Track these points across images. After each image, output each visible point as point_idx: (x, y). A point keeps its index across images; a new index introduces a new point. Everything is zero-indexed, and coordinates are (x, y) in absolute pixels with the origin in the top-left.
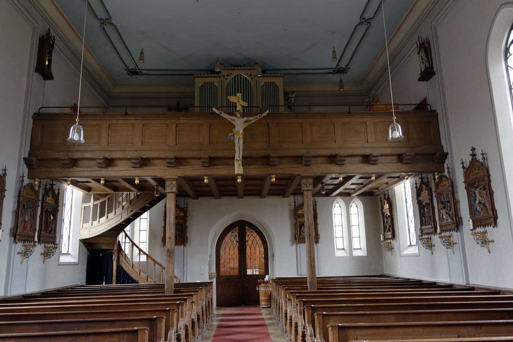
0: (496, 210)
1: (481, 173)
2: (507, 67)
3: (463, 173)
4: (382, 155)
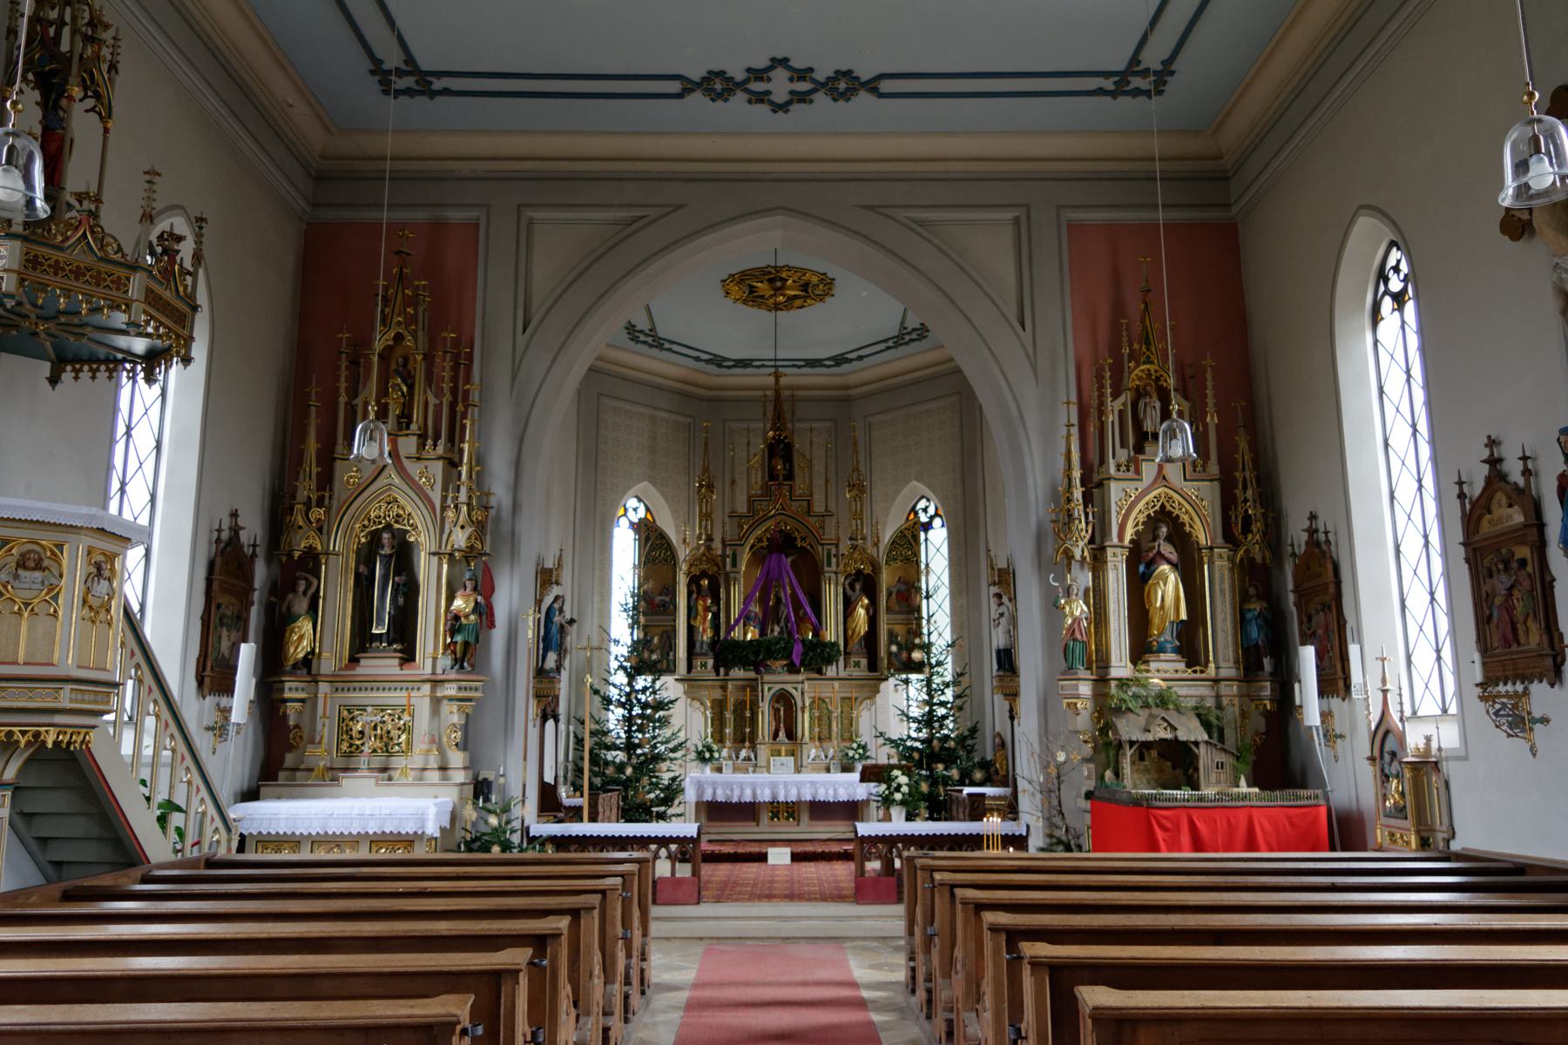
0: (1561, 635)
1: (1517, 517)
2: (1376, 342)
3: (1459, 514)
4: (1403, 322)
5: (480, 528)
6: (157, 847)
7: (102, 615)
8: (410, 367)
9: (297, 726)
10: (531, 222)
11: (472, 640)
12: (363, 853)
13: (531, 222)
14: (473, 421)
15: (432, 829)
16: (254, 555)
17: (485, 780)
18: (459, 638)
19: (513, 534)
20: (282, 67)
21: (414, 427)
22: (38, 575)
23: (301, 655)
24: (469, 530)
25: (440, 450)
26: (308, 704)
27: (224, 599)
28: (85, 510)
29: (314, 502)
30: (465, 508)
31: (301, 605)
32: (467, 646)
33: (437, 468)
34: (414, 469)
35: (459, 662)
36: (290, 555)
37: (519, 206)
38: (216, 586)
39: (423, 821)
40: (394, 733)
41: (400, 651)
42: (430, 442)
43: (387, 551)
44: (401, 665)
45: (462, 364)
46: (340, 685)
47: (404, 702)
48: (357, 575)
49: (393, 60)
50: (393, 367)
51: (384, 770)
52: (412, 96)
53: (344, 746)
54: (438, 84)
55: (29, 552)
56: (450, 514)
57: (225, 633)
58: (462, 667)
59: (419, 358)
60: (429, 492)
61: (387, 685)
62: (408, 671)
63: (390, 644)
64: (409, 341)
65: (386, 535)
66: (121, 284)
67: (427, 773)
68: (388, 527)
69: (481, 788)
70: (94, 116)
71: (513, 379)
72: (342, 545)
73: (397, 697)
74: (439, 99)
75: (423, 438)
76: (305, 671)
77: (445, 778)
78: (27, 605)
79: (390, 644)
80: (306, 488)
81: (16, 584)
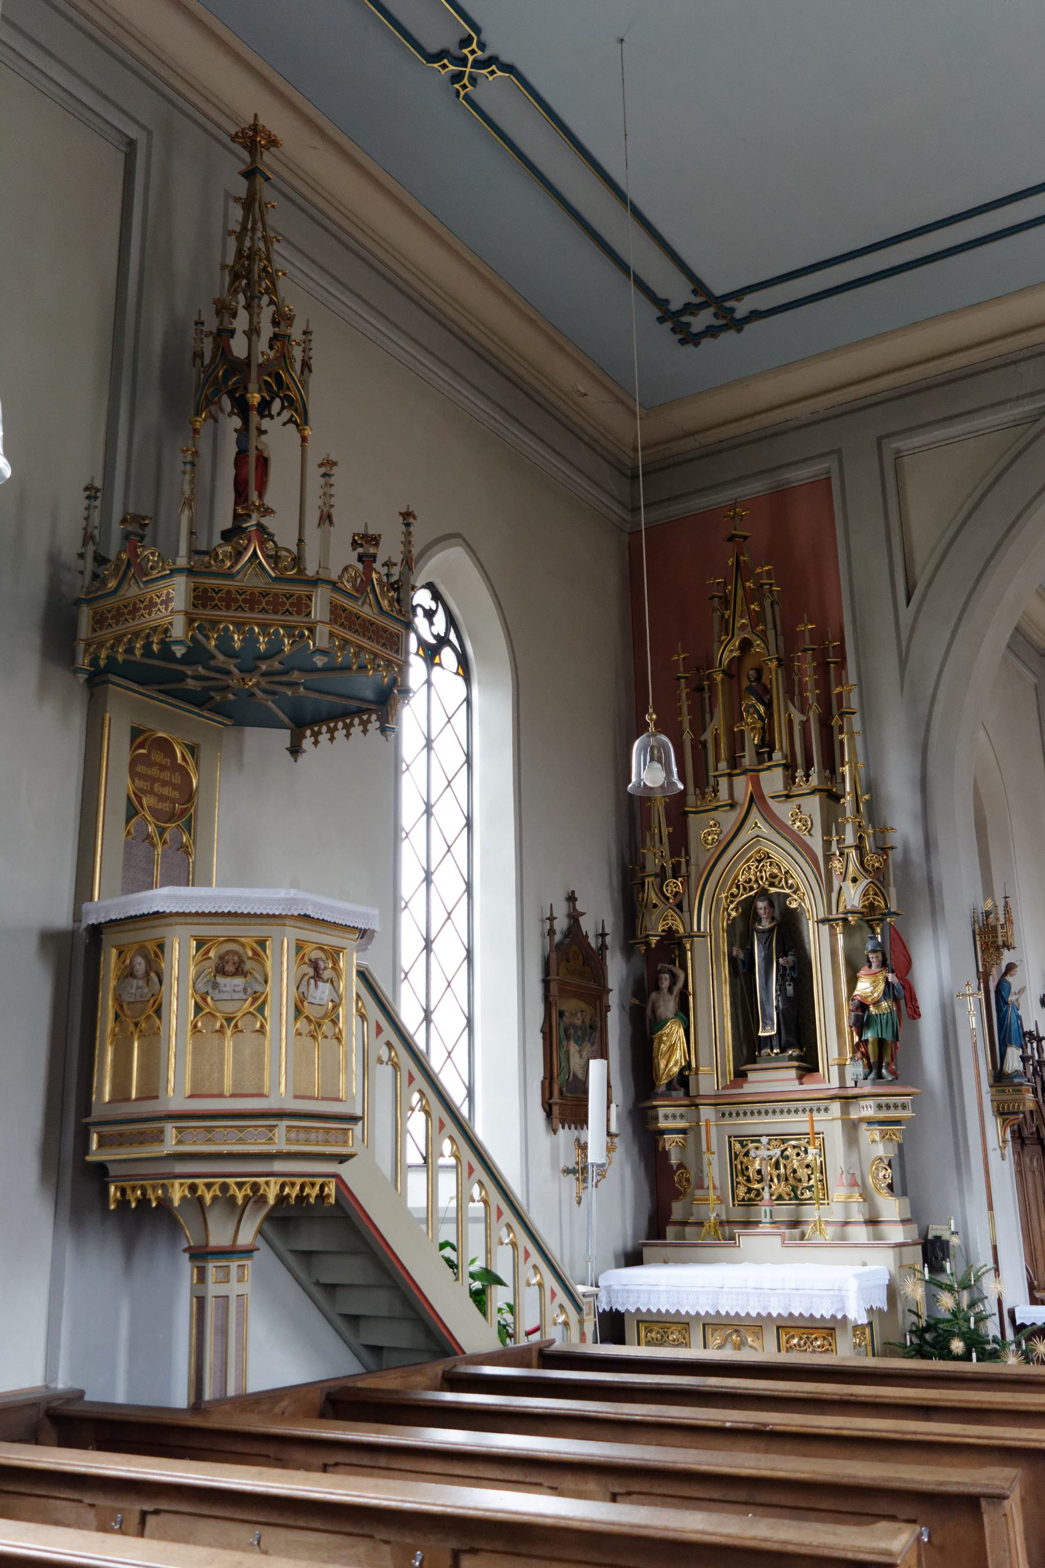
5: (879, 878)
6: (473, 1333)
7: (327, 1027)
8: (765, 680)
9: (681, 1166)
10: (898, 456)
11: (888, 1036)
12: (764, 1351)
13: (898, 456)
14: (851, 738)
15: (857, 1314)
16: (603, 947)
17: (938, 1238)
18: (869, 1035)
19: (930, 882)
20: (561, 349)
21: (777, 756)
22: (239, 981)
23: (676, 1069)
24: (863, 883)
25: (814, 781)
26: (691, 1136)
27: (570, 1005)
28: (282, 893)
29: (669, 872)
30: (853, 853)
31: (668, 1005)
32: (885, 1047)
33: (813, 805)
34: (784, 811)
35: (875, 1068)
36: (648, 944)
37: (880, 440)
38: (554, 988)
39: (842, 1300)
40: (802, 1173)
41: (799, 1058)
42: (800, 773)
43: (765, 924)
44: (800, 1078)
45: (830, 662)
46: (727, 1109)
47: (806, 1128)
48: (732, 961)
49: (679, 293)
50: (745, 683)
51: (795, 1224)
52: (714, 336)
53: (741, 1191)
54: (742, 308)
55: (228, 952)
56: (836, 864)
57: (573, 1048)
58: (880, 1076)
59: (773, 665)
60: (807, 839)
61: (785, 1106)
62: (810, 1086)
63: (783, 1050)
64: (758, 644)
65: (761, 904)
66: (302, 606)
67: (850, 1229)
68: (763, 893)
69: (934, 1252)
70: (292, 427)
71: (903, 664)
72: (708, 926)
73: (796, 1123)
74: (748, 328)
75: (789, 767)
76: (681, 1093)
77: (878, 1237)
78: (229, 1020)
79: (783, 1050)
80: (656, 856)
81: (217, 996)
